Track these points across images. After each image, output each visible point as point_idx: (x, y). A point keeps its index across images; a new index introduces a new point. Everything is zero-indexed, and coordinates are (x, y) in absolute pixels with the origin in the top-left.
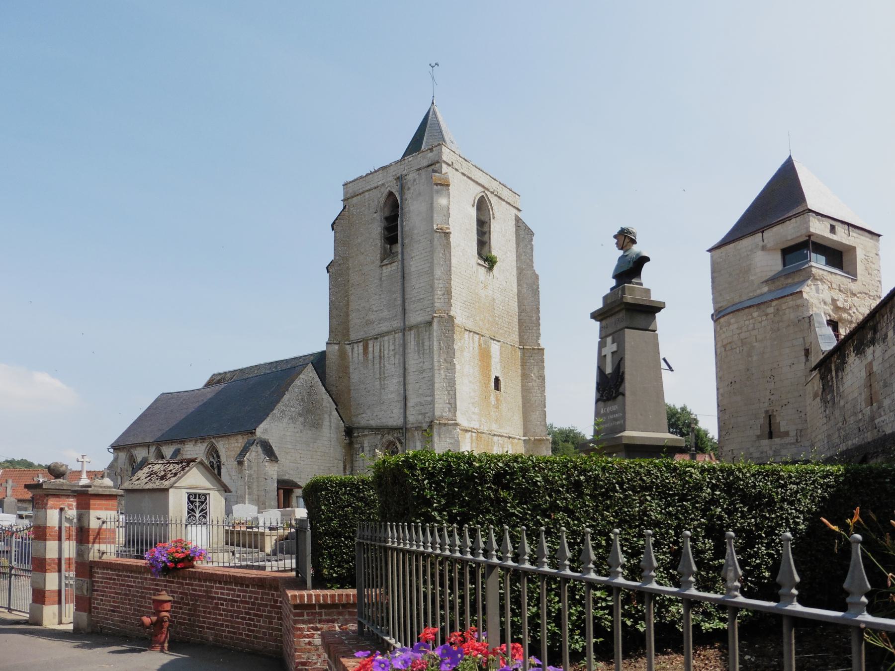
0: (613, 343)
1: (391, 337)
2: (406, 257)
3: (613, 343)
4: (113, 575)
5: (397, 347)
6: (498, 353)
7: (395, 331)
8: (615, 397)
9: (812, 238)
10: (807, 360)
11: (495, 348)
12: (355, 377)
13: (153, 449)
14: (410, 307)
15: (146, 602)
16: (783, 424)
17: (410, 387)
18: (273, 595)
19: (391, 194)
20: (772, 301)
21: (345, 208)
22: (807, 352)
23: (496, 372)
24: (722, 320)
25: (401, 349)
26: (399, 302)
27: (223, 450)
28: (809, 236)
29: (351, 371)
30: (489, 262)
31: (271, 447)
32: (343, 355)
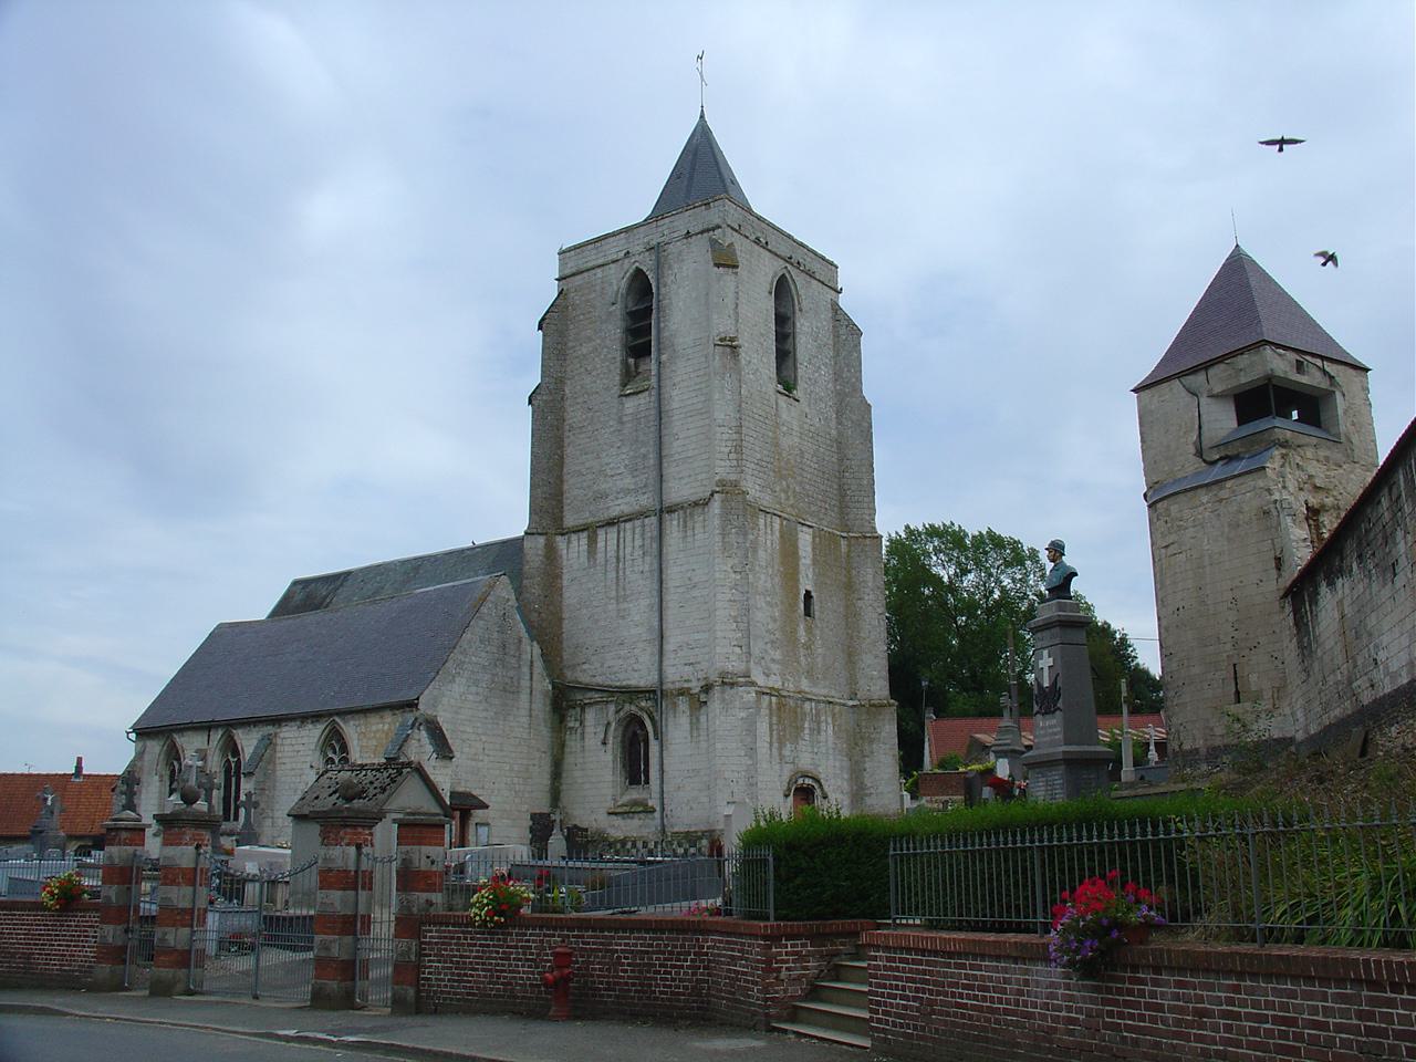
0: (1049, 657)
1: (638, 523)
2: (666, 383)
3: (1049, 657)
4: (456, 932)
5: (648, 542)
6: (809, 549)
7: (642, 514)
8: (1053, 712)
9: (1274, 382)
10: (1280, 576)
11: (805, 539)
12: (571, 595)
13: (217, 735)
14: (670, 470)
15: (510, 965)
16: (1253, 678)
17: (670, 615)
18: (698, 940)
19: (639, 274)
20: (1226, 479)
21: (560, 293)
22: (1279, 563)
23: (806, 584)
24: (1159, 505)
25: (655, 545)
26: (652, 461)
27: (355, 736)
28: (1270, 379)
29: (565, 583)
30: (787, 385)
31: (441, 729)
32: (551, 554)
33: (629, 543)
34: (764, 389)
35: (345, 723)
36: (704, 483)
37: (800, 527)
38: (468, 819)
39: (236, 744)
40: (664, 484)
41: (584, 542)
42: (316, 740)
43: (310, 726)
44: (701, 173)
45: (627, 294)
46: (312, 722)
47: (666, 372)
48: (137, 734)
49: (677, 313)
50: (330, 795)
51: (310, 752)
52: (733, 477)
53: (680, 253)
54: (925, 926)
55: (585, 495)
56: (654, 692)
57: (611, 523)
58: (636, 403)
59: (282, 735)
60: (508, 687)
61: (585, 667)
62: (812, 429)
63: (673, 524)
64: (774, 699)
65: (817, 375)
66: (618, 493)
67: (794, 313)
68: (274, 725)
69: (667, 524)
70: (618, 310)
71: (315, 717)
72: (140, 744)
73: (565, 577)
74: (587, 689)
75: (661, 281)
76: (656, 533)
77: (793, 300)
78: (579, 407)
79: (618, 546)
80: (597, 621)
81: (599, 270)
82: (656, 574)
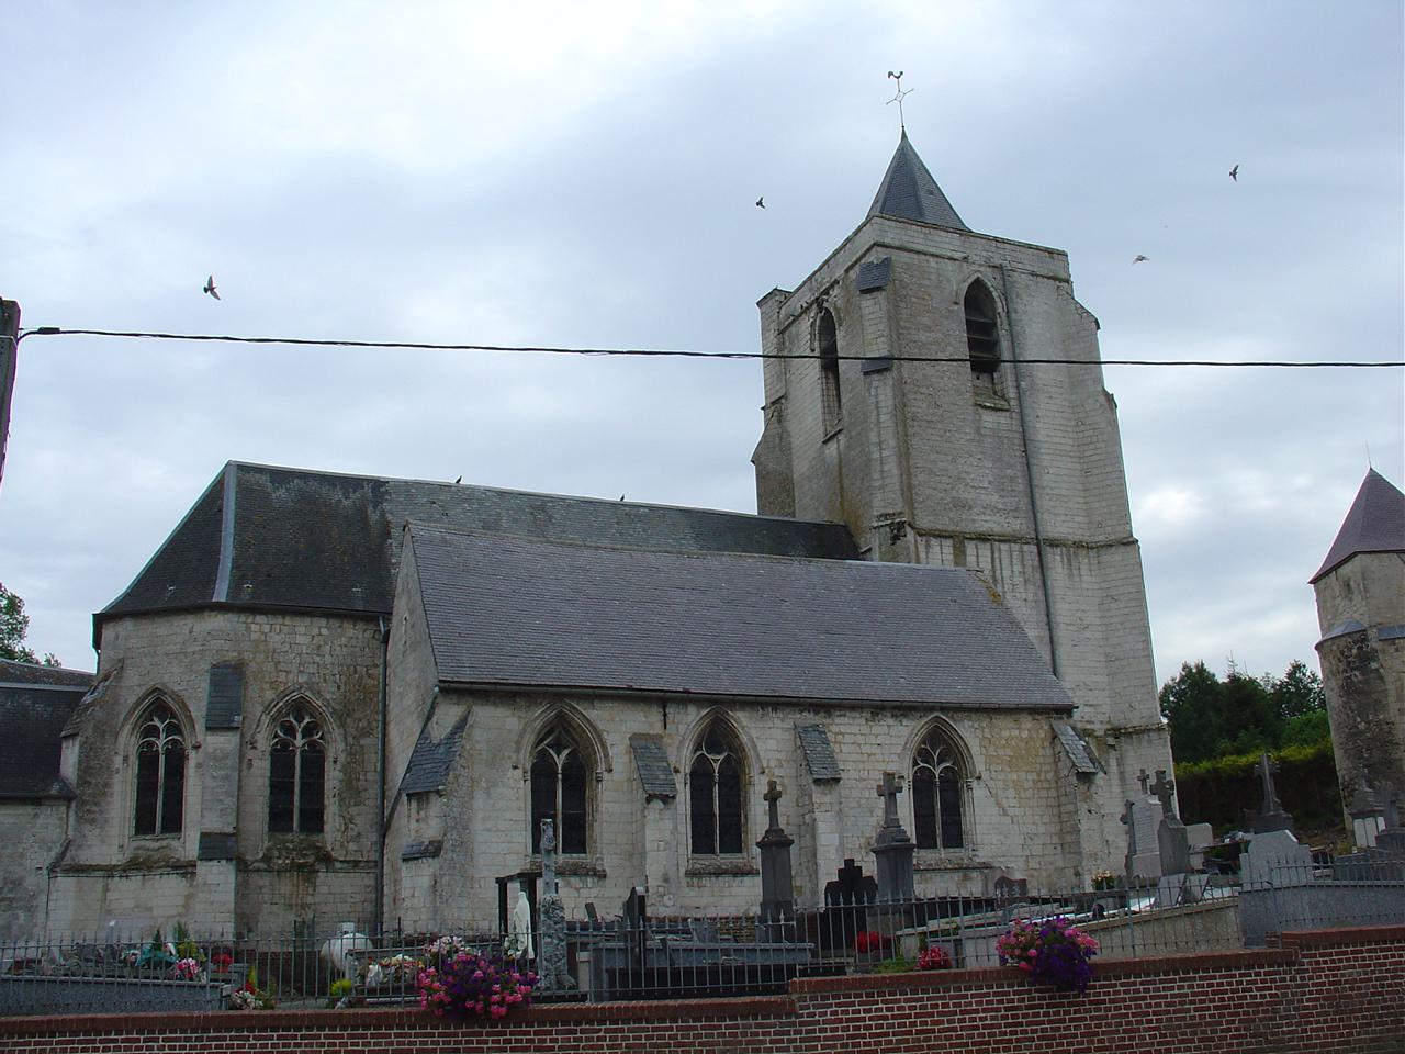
14: (1044, 503)
33: (1006, 561)
35: (955, 721)
36: (1082, 525)
43: (891, 721)
44: (908, 190)
49: (932, 331)
51: (896, 758)
54: (1016, 971)
55: (942, 499)
57: (982, 538)
58: (996, 419)
68: (816, 713)
71: (902, 710)
76: (1036, 563)
79: (993, 566)
82: (1043, 606)
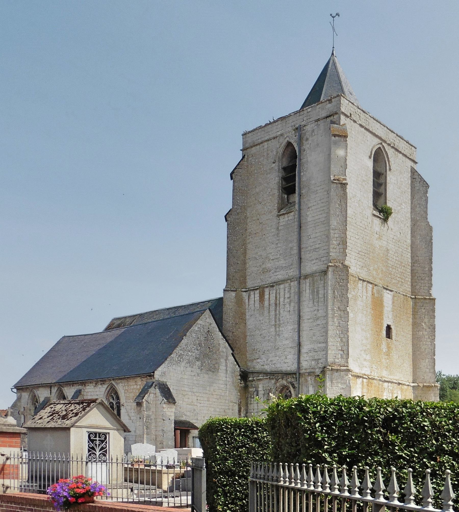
1: (287, 285)
2: (303, 207)
5: (292, 295)
6: (390, 303)
11: (388, 297)
19: (289, 144)
25: (296, 297)
26: (295, 251)
29: (247, 317)
32: (239, 302)
34: (364, 212)
37: (385, 291)
38: (188, 434)
39: (64, 395)
40: (302, 264)
41: (257, 295)
42: (103, 393)
45: (282, 158)
46: (101, 384)
47: (304, 200)
48: (17, 389)
50: (48, 417)
52: (340, 258)
53: (313, 131)
56: (295, 374)
59: (86, 390)
60: (211, 369)
61: (259, 360)
62: (395, 238)
63: (306, 285)
64: (365, 380)
65: (399, 208)
66: (276, 269)
67: (386, 171)
69: (303, 286)
70: (275, 166)
72: (19, 394)
73: (247, 314)
74: (259, 373)
75: (302, 148)
77: (386, 163)
78: (254, 222)
80: (265, 337)
81: (266, 143)
